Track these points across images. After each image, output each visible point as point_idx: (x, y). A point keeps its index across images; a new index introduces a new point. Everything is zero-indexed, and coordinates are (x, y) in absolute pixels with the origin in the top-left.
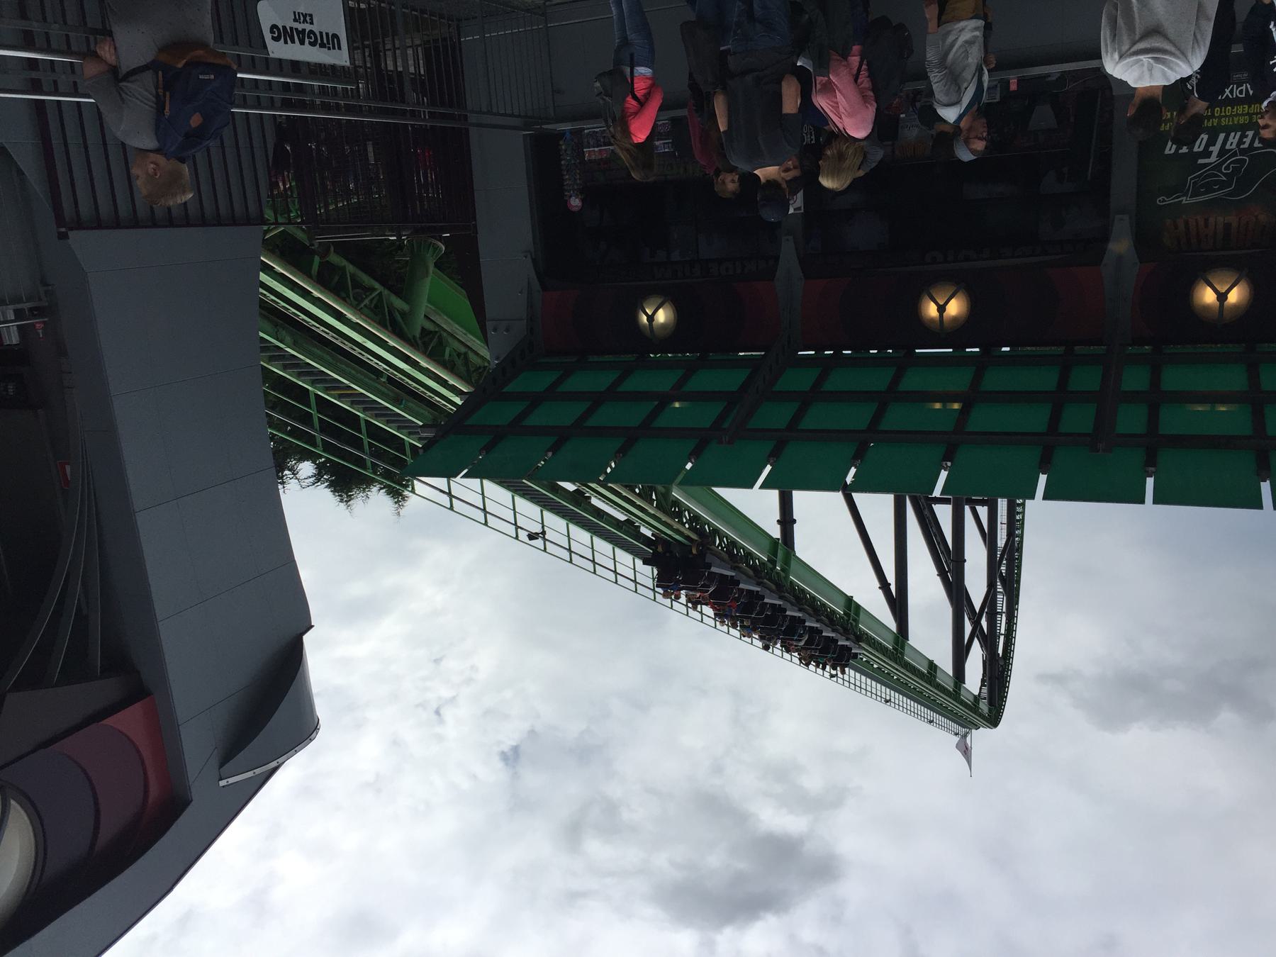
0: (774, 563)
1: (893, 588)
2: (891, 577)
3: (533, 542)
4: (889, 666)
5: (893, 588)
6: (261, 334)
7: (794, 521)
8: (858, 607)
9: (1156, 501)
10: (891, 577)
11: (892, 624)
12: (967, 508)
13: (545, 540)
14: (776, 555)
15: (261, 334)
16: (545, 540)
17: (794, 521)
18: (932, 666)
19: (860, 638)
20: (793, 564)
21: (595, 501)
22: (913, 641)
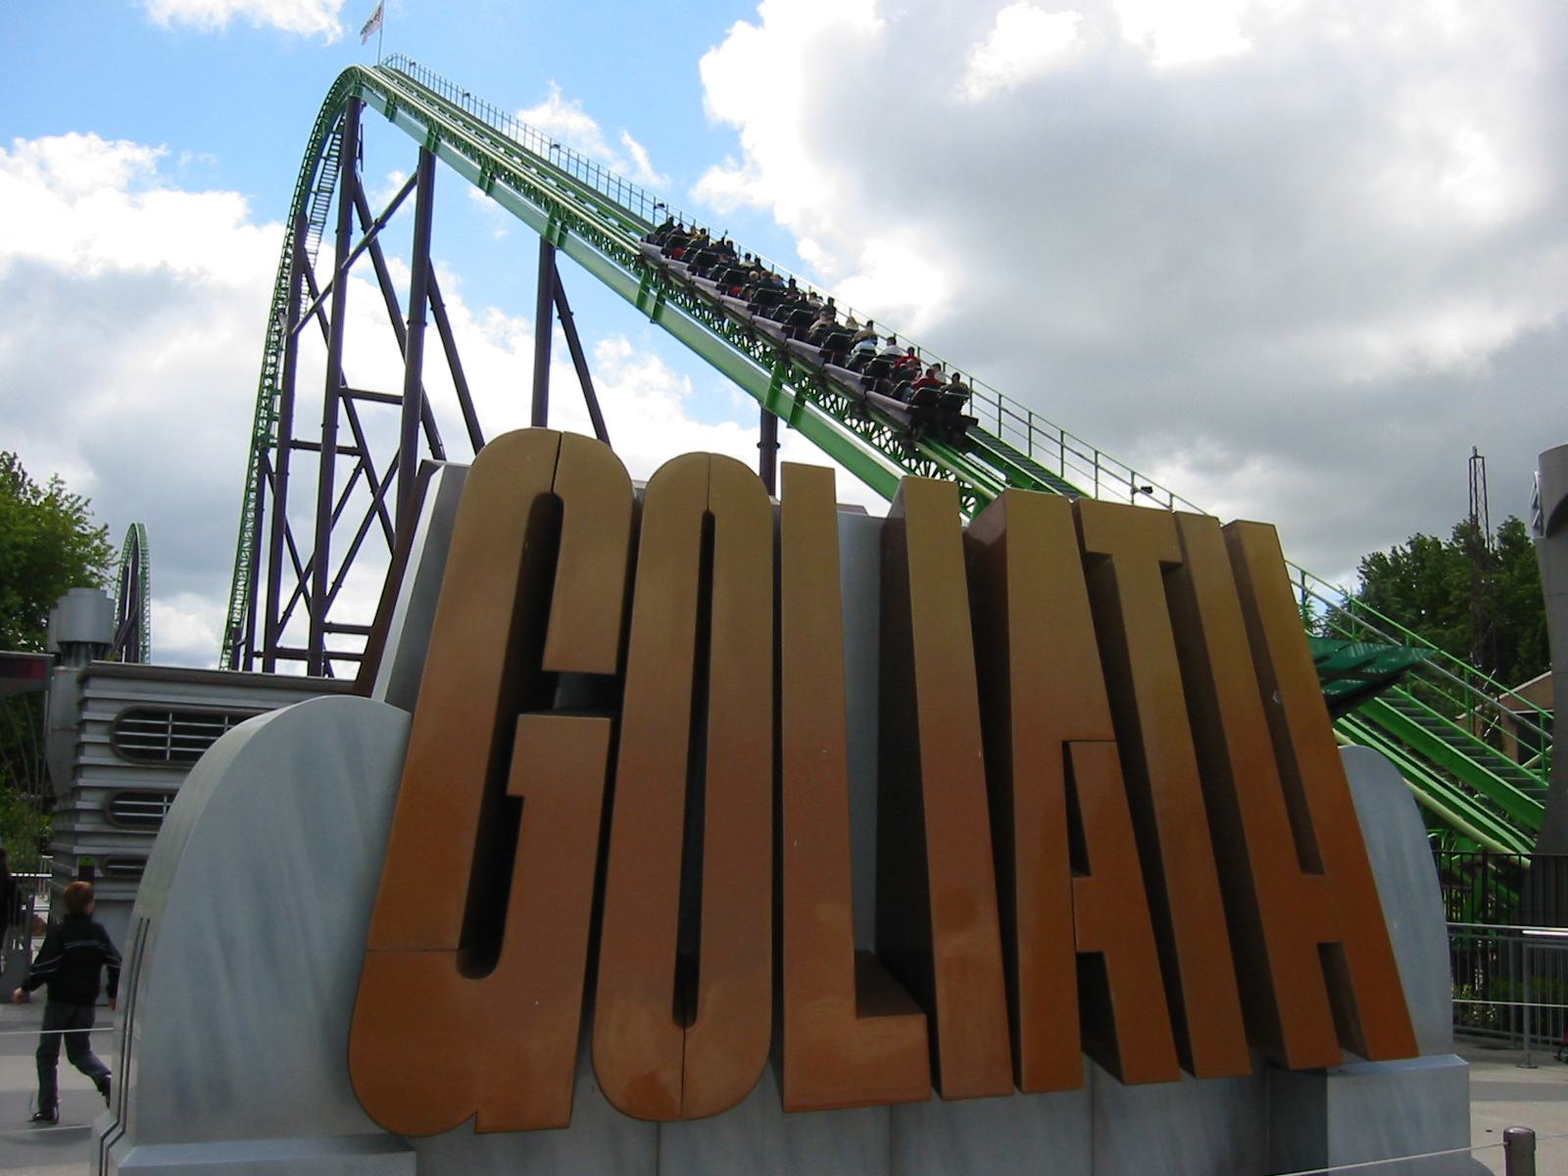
0: (563, 228)
1: (555, 313)
2: (558, 331)
3: (1147, 484)
4: (566, 200)
5: (555, 313)
6: (1543, 807)
7: (572, 314)
8: (386, 115)
9: (42, 1034)
10: (558, 331)
11: (561, 259)
12: (341, 400)
13: (1132, 485)
14: (490, 183)
15: (1543, 807)
16: (1132, 485)
17: (572, 314)
18: (391, 114)
19: (642, 261)
20: (545, 229)
21: (1002, 477)
22: (755, 408)
